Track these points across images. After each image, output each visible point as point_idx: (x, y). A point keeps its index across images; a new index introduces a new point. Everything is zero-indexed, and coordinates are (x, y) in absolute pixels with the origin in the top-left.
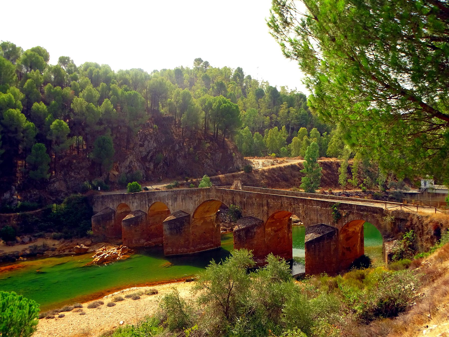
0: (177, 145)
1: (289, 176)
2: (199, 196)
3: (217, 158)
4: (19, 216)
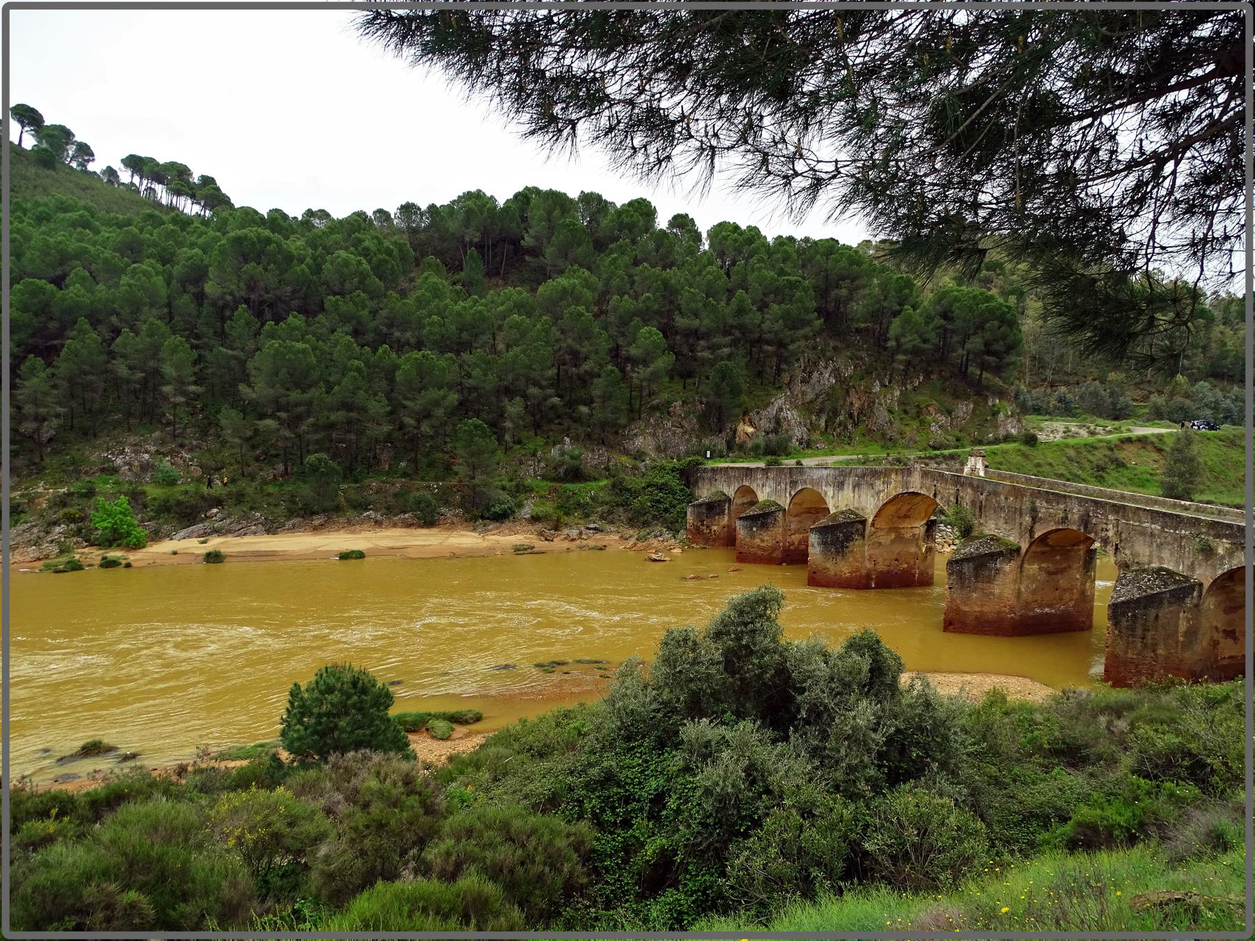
2: (889, 483)
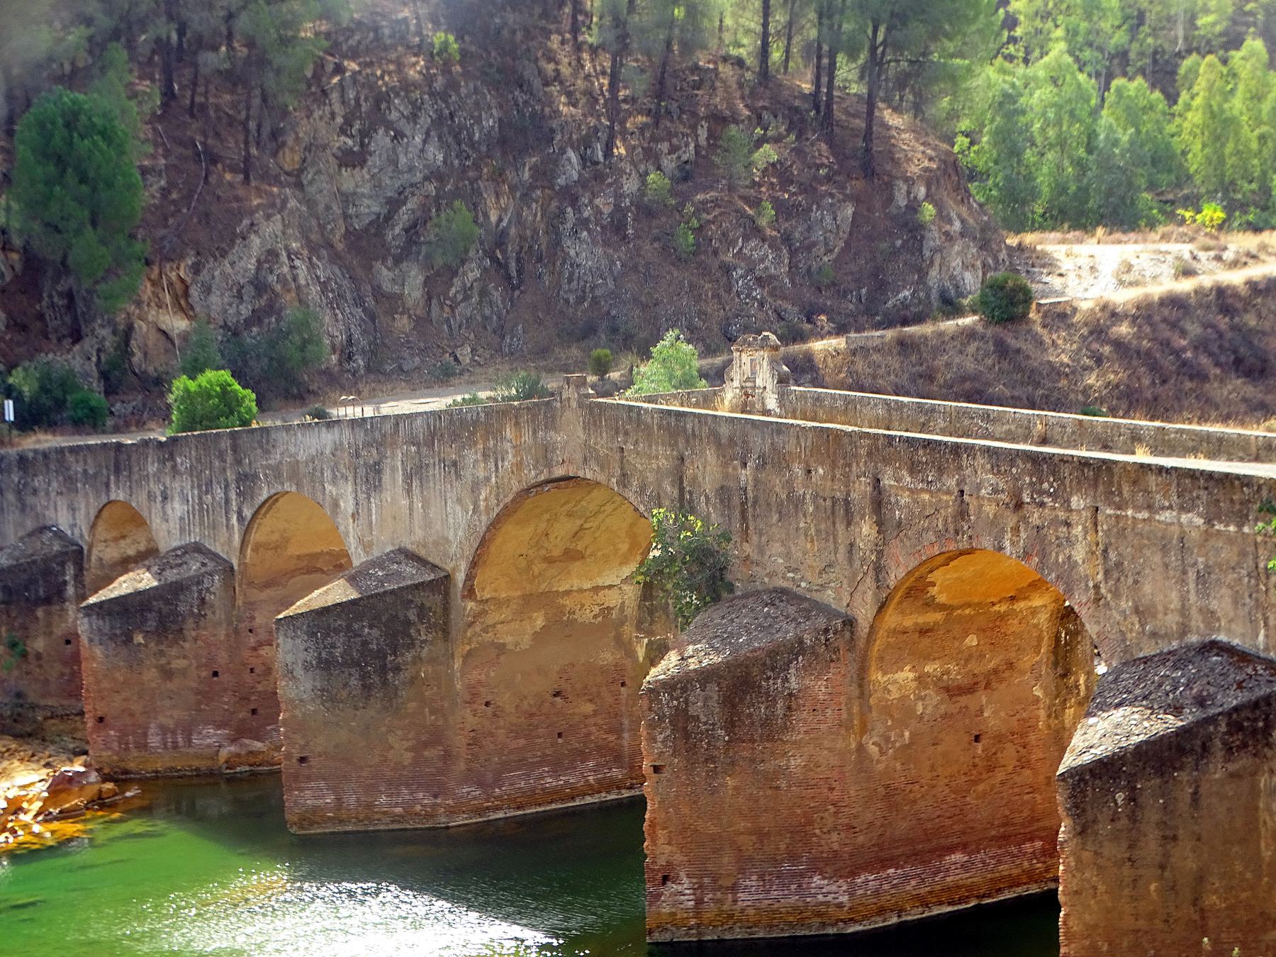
0: (571, 154)
2: (499, 457)
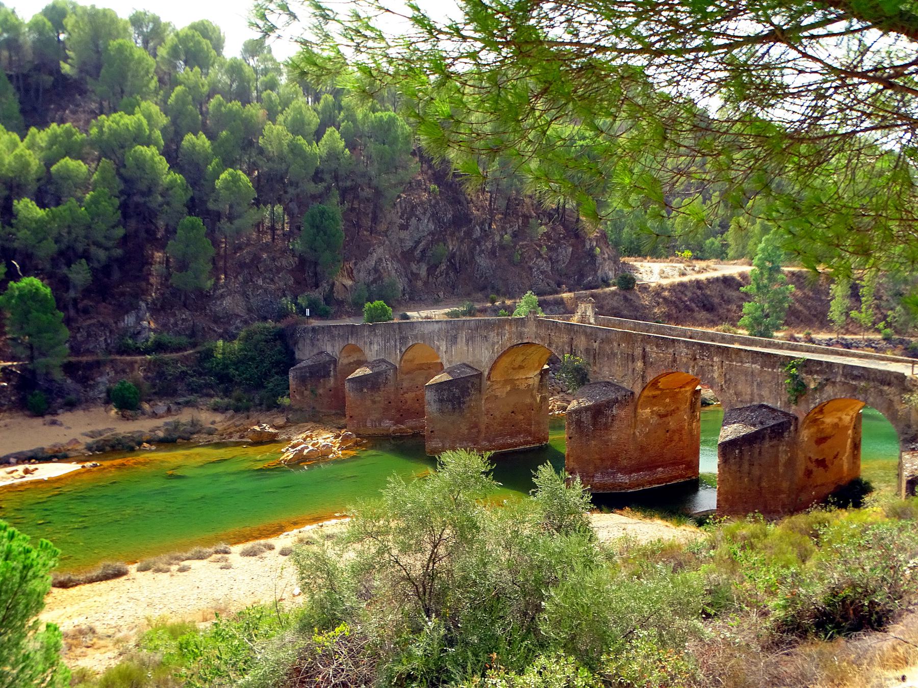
0: (478, 227)
1: (716, 300)
2: (502, 335)
3: (561, 257)
4: (150, 361)
